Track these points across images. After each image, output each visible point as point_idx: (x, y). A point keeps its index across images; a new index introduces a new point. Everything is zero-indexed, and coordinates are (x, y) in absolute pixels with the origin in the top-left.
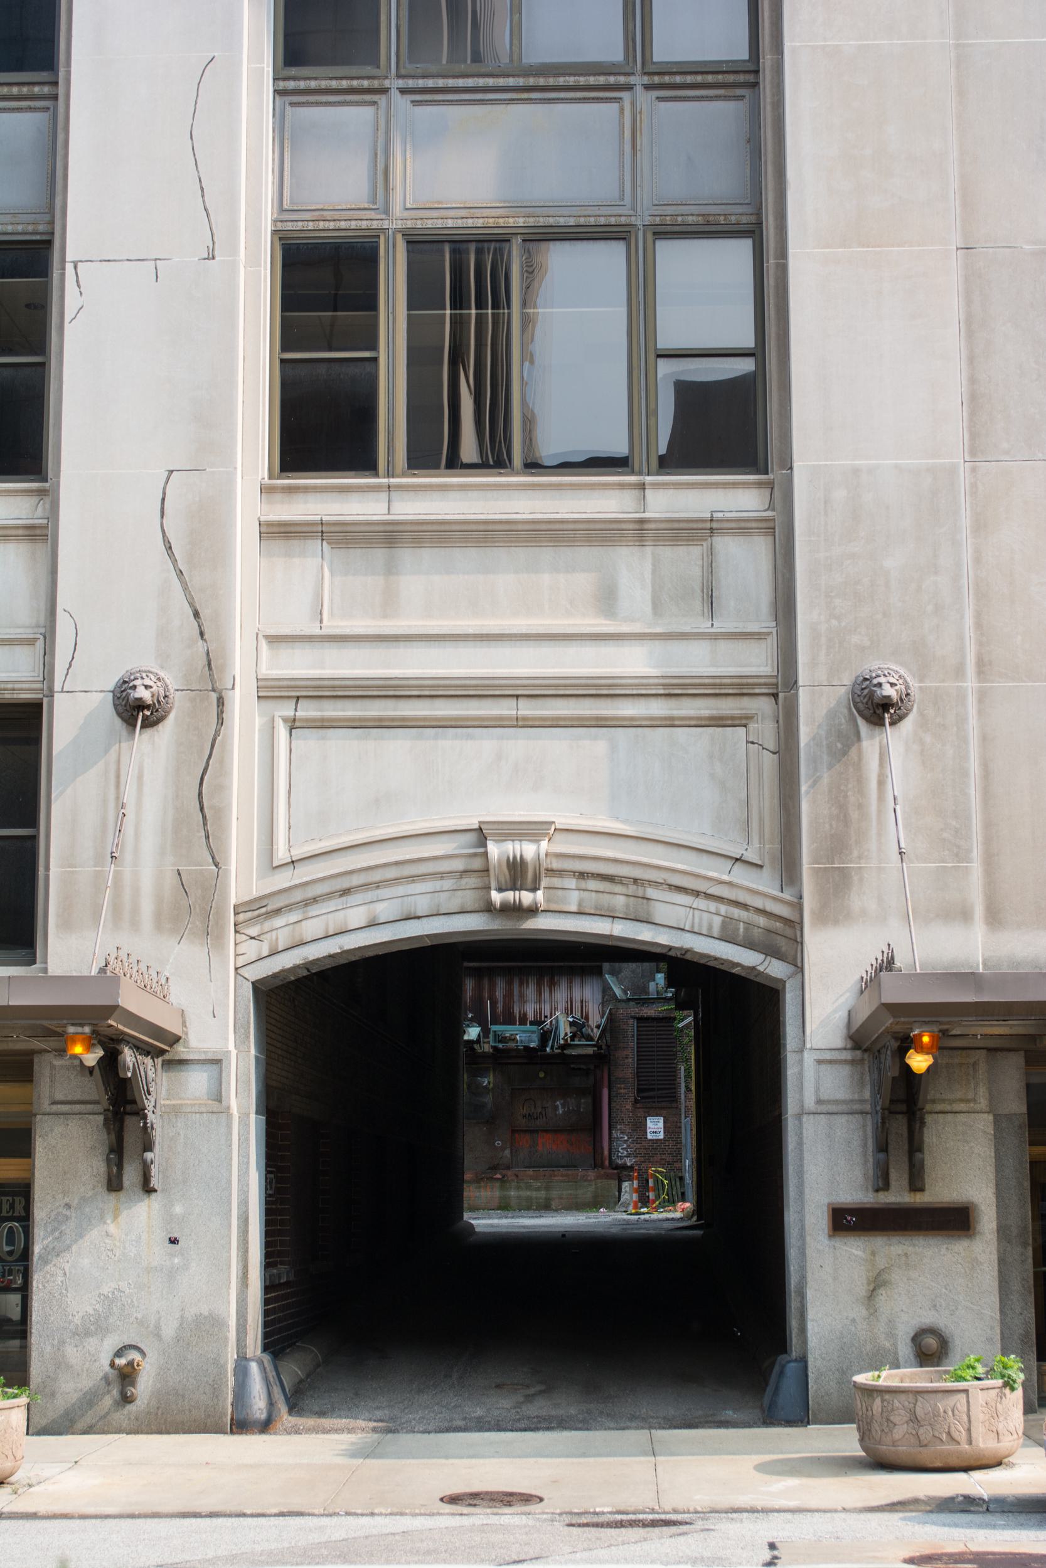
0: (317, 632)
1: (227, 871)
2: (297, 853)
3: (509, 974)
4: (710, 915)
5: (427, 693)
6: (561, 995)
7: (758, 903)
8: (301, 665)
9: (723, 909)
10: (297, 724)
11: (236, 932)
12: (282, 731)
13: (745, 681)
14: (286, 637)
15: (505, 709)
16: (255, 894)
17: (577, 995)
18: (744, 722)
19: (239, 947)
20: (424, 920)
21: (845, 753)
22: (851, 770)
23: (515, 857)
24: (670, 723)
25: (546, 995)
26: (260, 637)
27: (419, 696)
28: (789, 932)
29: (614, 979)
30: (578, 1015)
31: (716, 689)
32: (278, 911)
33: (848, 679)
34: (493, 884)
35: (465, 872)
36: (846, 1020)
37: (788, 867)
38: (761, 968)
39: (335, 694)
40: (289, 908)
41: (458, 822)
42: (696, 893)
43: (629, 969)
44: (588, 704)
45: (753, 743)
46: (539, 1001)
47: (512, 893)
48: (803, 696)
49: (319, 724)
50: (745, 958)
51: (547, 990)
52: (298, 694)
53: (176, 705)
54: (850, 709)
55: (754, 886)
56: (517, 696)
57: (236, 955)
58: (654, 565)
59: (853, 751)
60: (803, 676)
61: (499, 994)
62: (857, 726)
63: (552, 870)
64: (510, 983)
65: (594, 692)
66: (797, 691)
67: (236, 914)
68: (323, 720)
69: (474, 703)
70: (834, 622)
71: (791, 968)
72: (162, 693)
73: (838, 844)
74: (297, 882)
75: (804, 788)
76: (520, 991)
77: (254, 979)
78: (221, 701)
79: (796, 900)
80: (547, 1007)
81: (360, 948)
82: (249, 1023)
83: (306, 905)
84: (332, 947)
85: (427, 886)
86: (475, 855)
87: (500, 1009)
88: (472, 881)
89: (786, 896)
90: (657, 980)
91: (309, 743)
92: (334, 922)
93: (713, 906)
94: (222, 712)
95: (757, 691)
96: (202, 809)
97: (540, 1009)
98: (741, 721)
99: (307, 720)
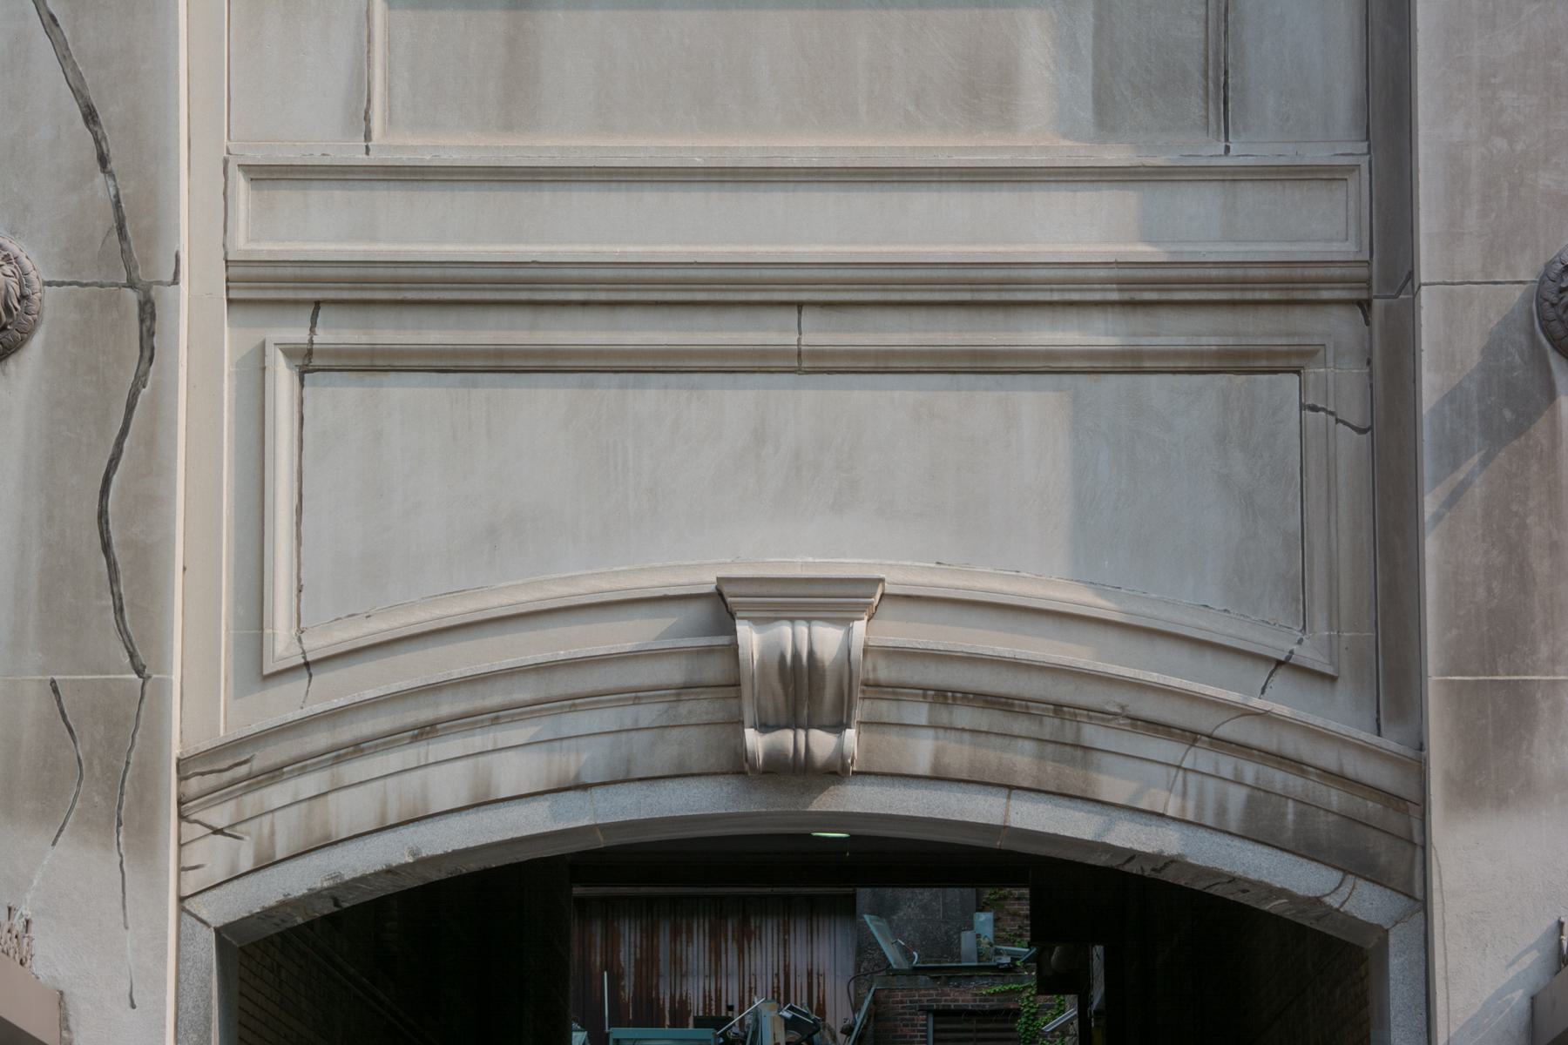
0: (360, 158)
1: (165, 686)
2: (317, 645)
3: (647, 910)
4: (1226, 784)
5: (602, 296)
6: (764, 959)
7: (1327, 757)
8: (323, 231)
9: (1250, 770)
10: (316, 362)
11: (182, 817)
12: (282, 376)
13: (1298, 272)
14: (291, 168)
15: (774, 333)
16: (223, 734)
17: (799, 958)
18: (1295, 362)
19: (186, 850)
20: (598, 793)
21: (1520, 429)
22: (1535, 468)
23: (796, 655)
24: (1130, 363)
25: (731, 959)
26: (232, 167)
27: (584, 304)
28: (1395, 822)
29: (883, 924)
30: (801, 1003)
31: (1232, 289)
32: (274, 774)
33: (1527, 268)
34: (749, 714)
35: (685, 690)
36: (1526, 1018)
37: (1393, 682)
38: (1333, 901)
39: (400, 296)
40: (301, 765)
41: (671, 579)
42: (1192, 737)
43: (916, 902)
44: (956, 321)
45: (1314, 409)
46: (716, 971)
47: (789, 734)
48: (1429, 306)
49: (364, 362)
50: (1301, 878)
51: (732, 948)
52: (318, 295)
53: (47, 316)
54: (1533, 334)
55: (1319, 721)
56: (800, 305)
57: (182, 869)
58: (1098, 16)
59: (1540, 428)
60: (1429, 262)
61: (627, 956)
62: (1549, 371)
63: (877, 685)
64: (650, 934)
65: (967, 296)
66: (1415, 294)
67: (182, 778)
68: (373, 352)
69: (704, 318)
70: (1501, 143)
71: (1400, 903)
72: (15, 289)
73: (1502, 633)
74: (319, 708)
75: (1430, 504)
76: (673, 952)
77: (219, 920)
78: (148, 311)
79: (1410, 753)
80: (734, 986)
81: (456, 853)
82: (208, 1019)
83: (338, 760)
84: (393, 851)
85: (606, 718)
86: (709, 650)
87: (628, 991)
88: (700, 708)
89: (1389, 743)
90: (978, 928)
91: (339, 398)
92: (398, 797)
93: (1227, 764)
94: (152, 334)
95: (1325, 295)
96: (106, 547)
97: (718, 991)
98: (1288, 361)
99: (337, 353)
